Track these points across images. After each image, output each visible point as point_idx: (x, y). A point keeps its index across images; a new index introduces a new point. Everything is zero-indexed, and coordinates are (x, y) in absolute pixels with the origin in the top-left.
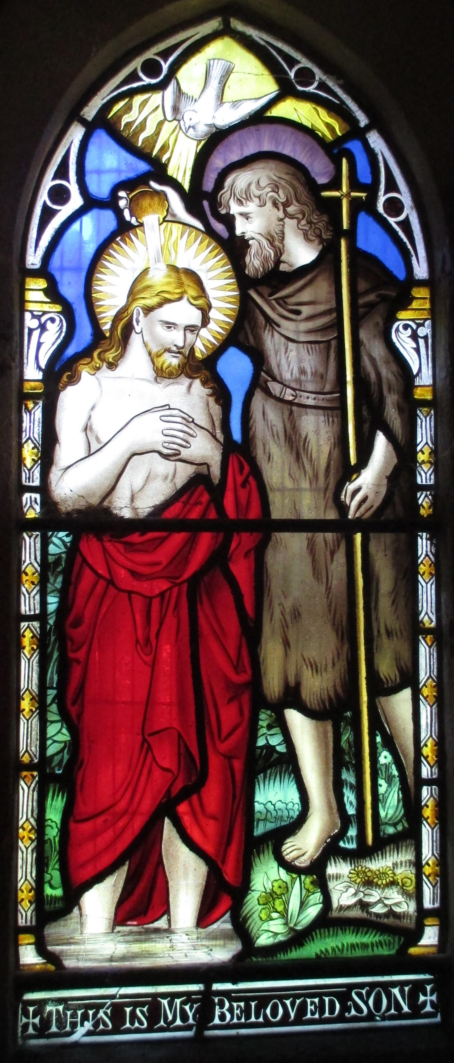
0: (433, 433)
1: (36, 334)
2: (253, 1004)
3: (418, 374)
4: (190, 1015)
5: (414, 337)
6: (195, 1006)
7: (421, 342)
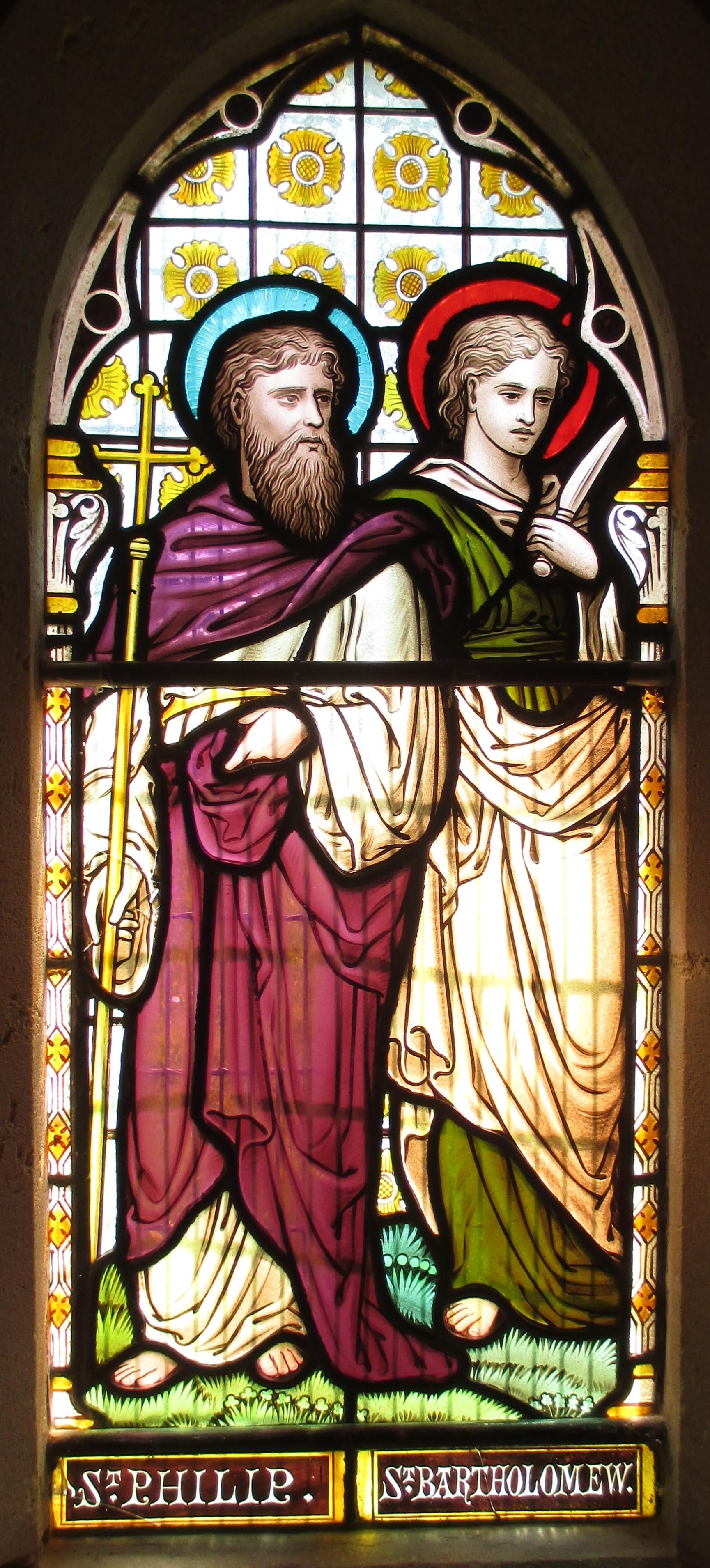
1: (64, 525)
2: (220, 1475)
3: (642, 586)
5: (641, 527)
7: (650, 535)
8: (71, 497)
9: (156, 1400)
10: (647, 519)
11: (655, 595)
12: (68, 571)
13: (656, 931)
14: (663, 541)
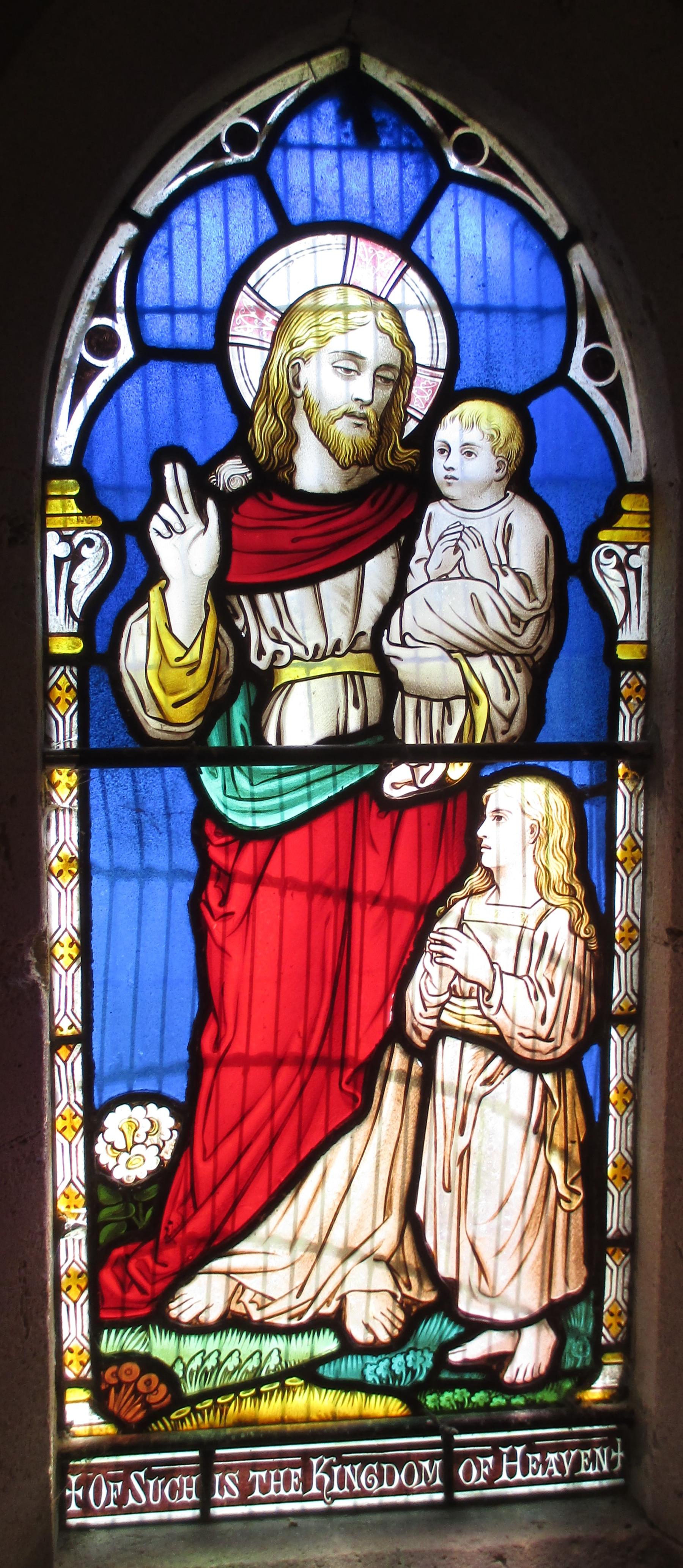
0: (626, 1280)
1: (66, 566)
5: (622, 567)
7: (631, 575)
8: (74, 534)
9: (302, 1337)
10: (627, 558)
11: (633, 631)
12: (72, 614)
13: (634, 912)
14: (644, 580)
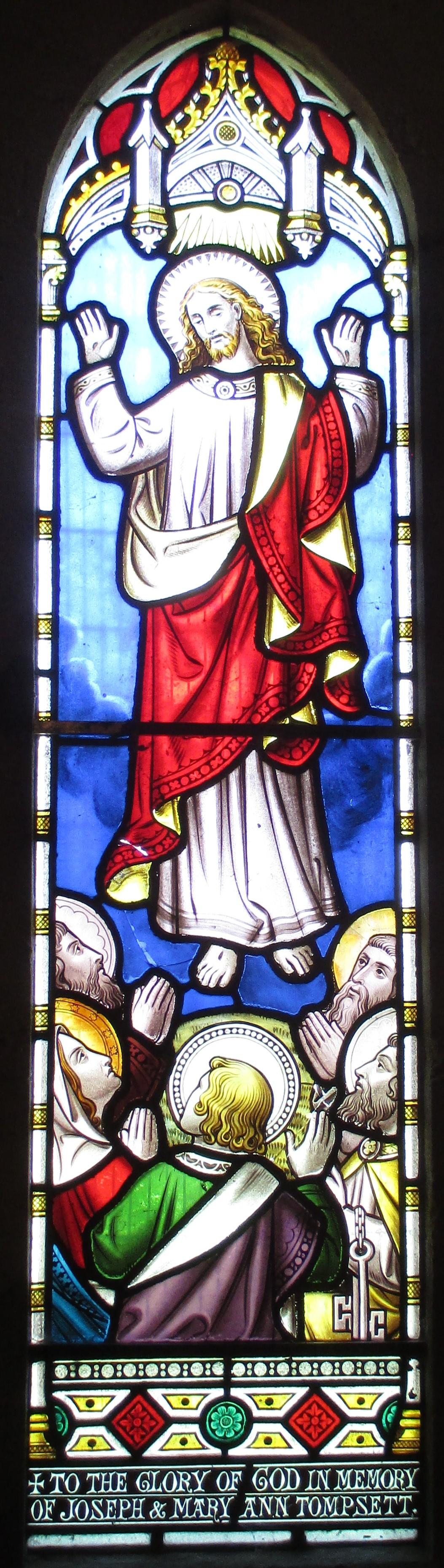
4: (200, 1483)
6: (415, 1470)
